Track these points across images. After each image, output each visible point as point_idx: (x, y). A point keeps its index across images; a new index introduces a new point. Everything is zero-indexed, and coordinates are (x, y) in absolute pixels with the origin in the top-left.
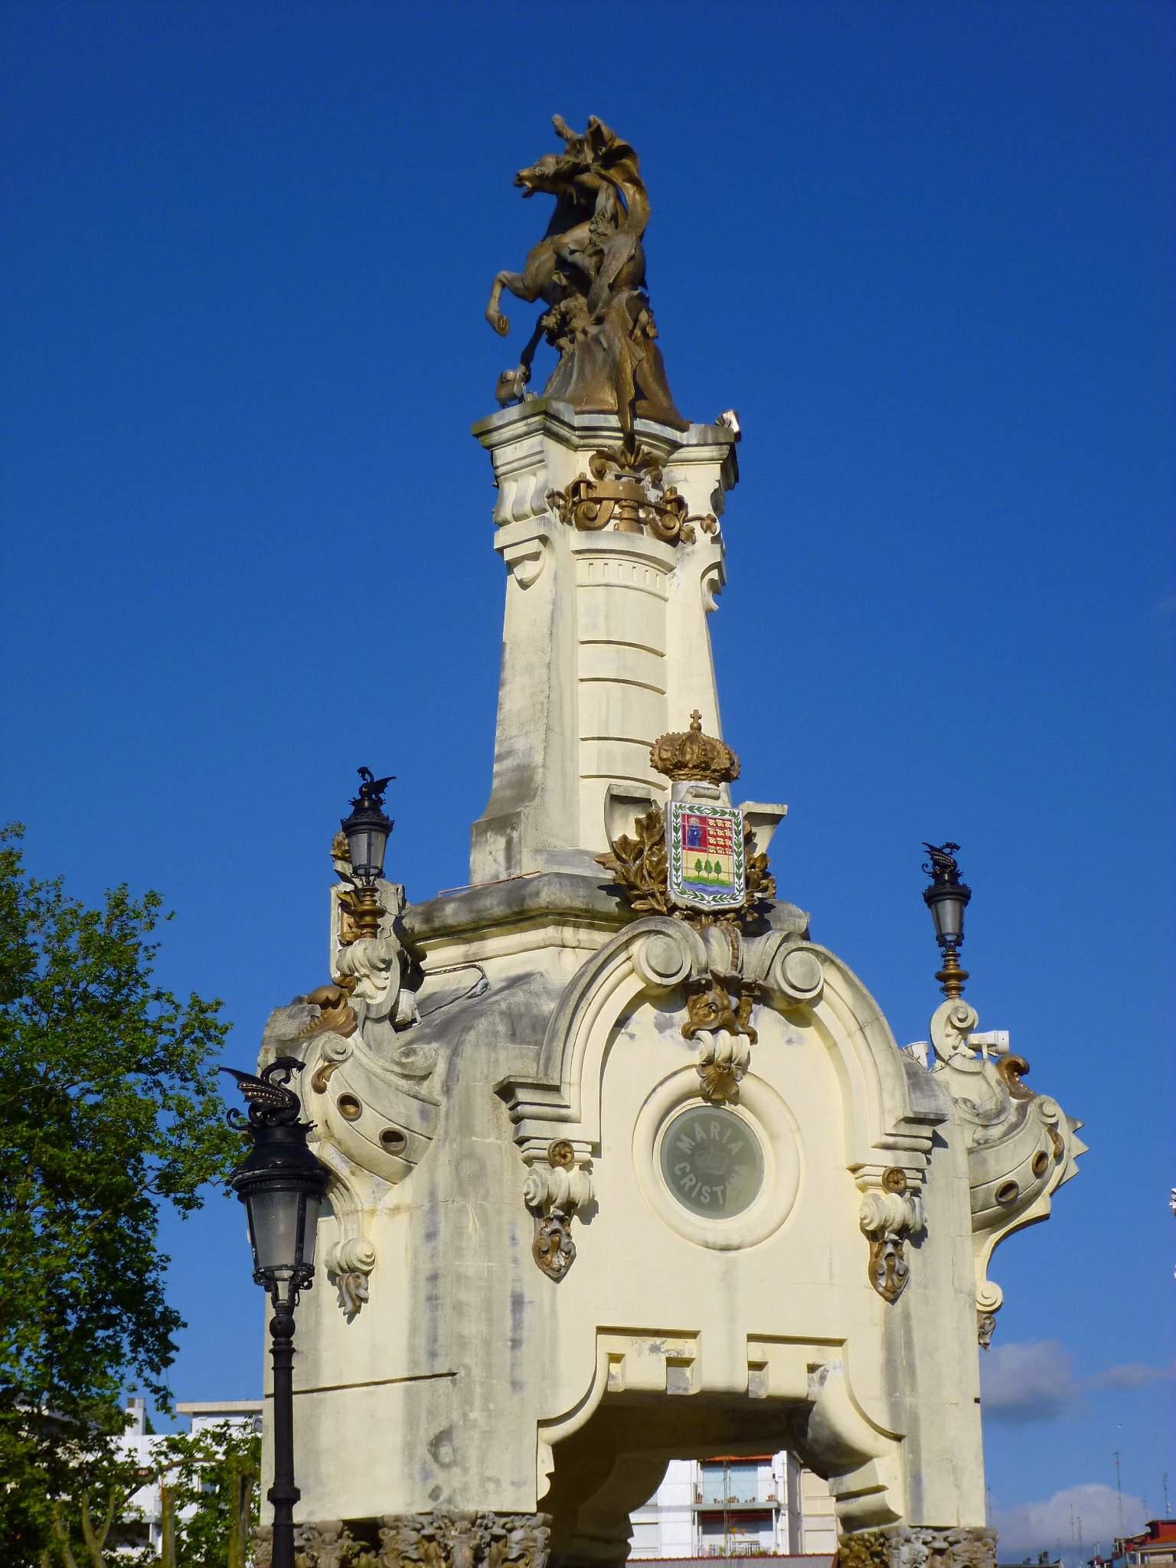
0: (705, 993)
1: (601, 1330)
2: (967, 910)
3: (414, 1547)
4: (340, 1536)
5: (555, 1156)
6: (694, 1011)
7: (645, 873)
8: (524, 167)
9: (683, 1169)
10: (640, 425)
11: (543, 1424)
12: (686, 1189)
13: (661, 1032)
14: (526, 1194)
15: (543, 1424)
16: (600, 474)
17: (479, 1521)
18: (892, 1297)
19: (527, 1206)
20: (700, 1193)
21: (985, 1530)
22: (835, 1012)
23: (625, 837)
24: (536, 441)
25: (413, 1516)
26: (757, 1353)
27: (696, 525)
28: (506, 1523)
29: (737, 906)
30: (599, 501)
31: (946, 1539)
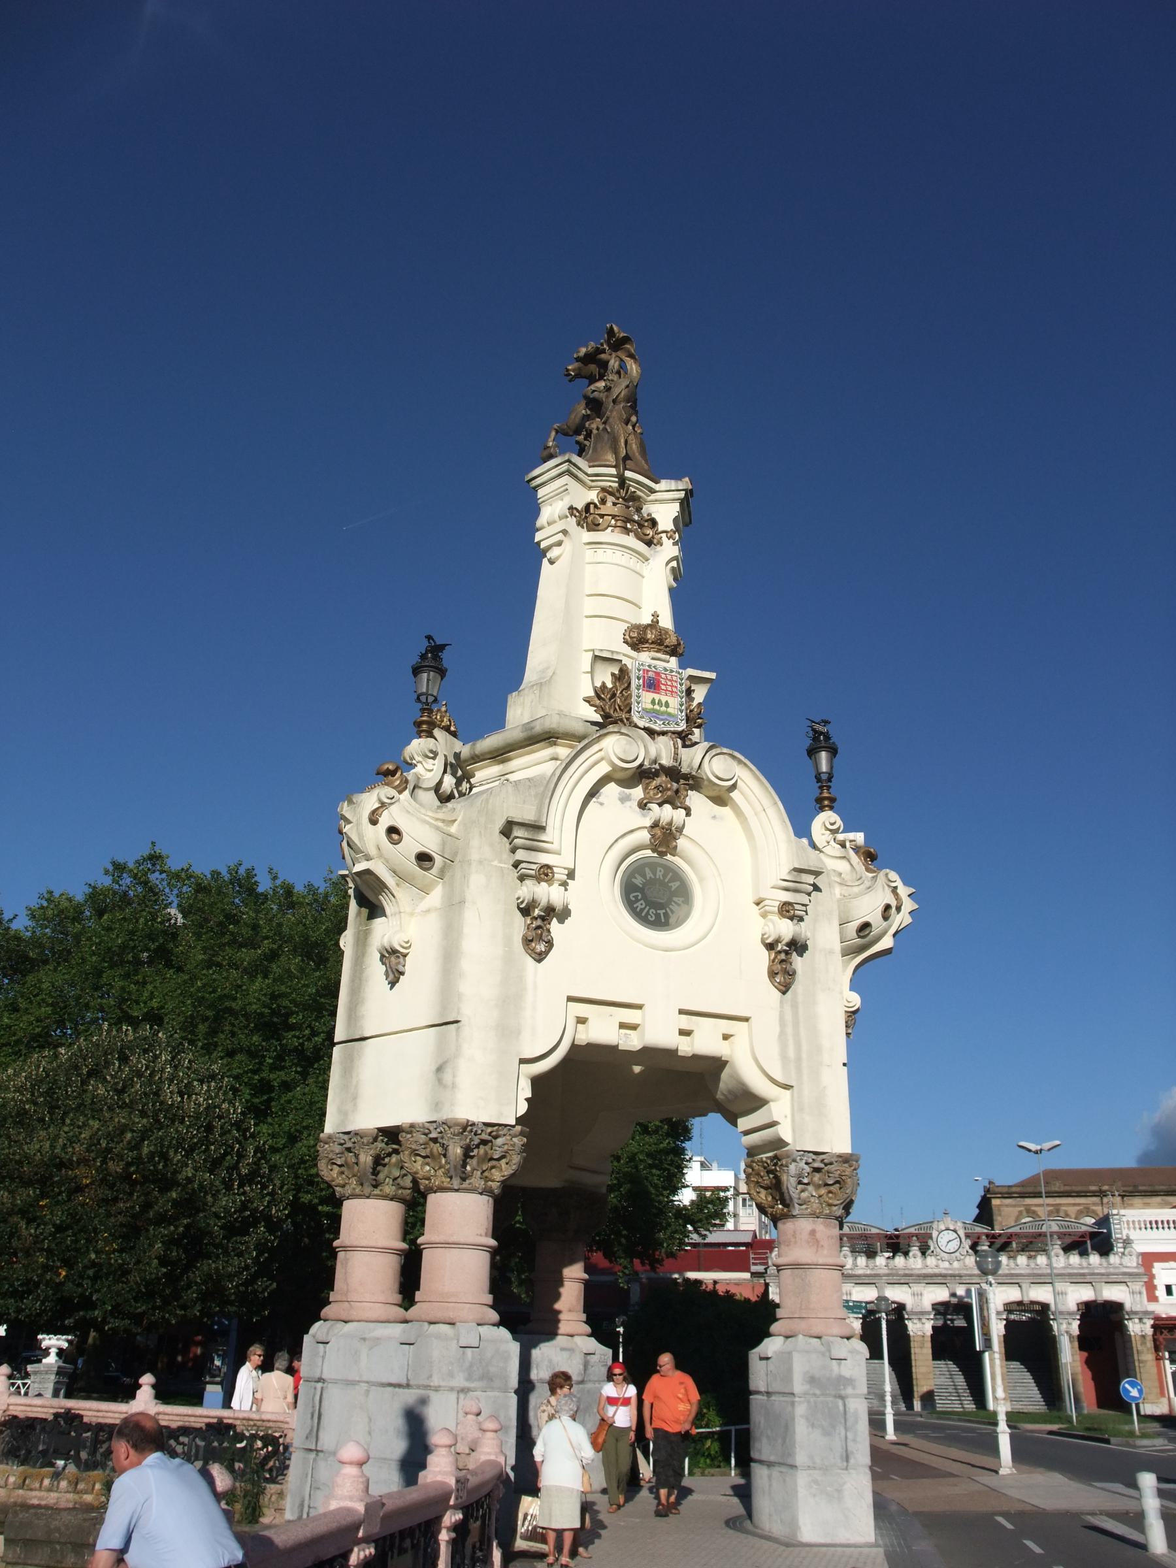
0: (654, 779)
1: (570, 999)
2: (835, 760)
3: (423, 1146)
4: (375, 1140)
5: (540, 875)
6: (647, 791)
7: (617, 707)
8: (570, 364)
9: (636, 897)
10: (628, 474)
11: (523, 1061)
12: (638, 910)
13: (623, 803)
14: (518, 899)
15: (523, 1061)
16: (603, 501)
17: (469, 1128)
18: (784, 989)
19: (519, 908)
20: (648, 913)
21: (851, 1155)
22: (749, 803)
23: (604, 683)
24: (566, 479)
25: (423, 1124)
26: (685, 1022)
27: (664, 535)
28: (492, 1132)
29: (680, 729)
30: (602, 516)
31: (822, 1161)
